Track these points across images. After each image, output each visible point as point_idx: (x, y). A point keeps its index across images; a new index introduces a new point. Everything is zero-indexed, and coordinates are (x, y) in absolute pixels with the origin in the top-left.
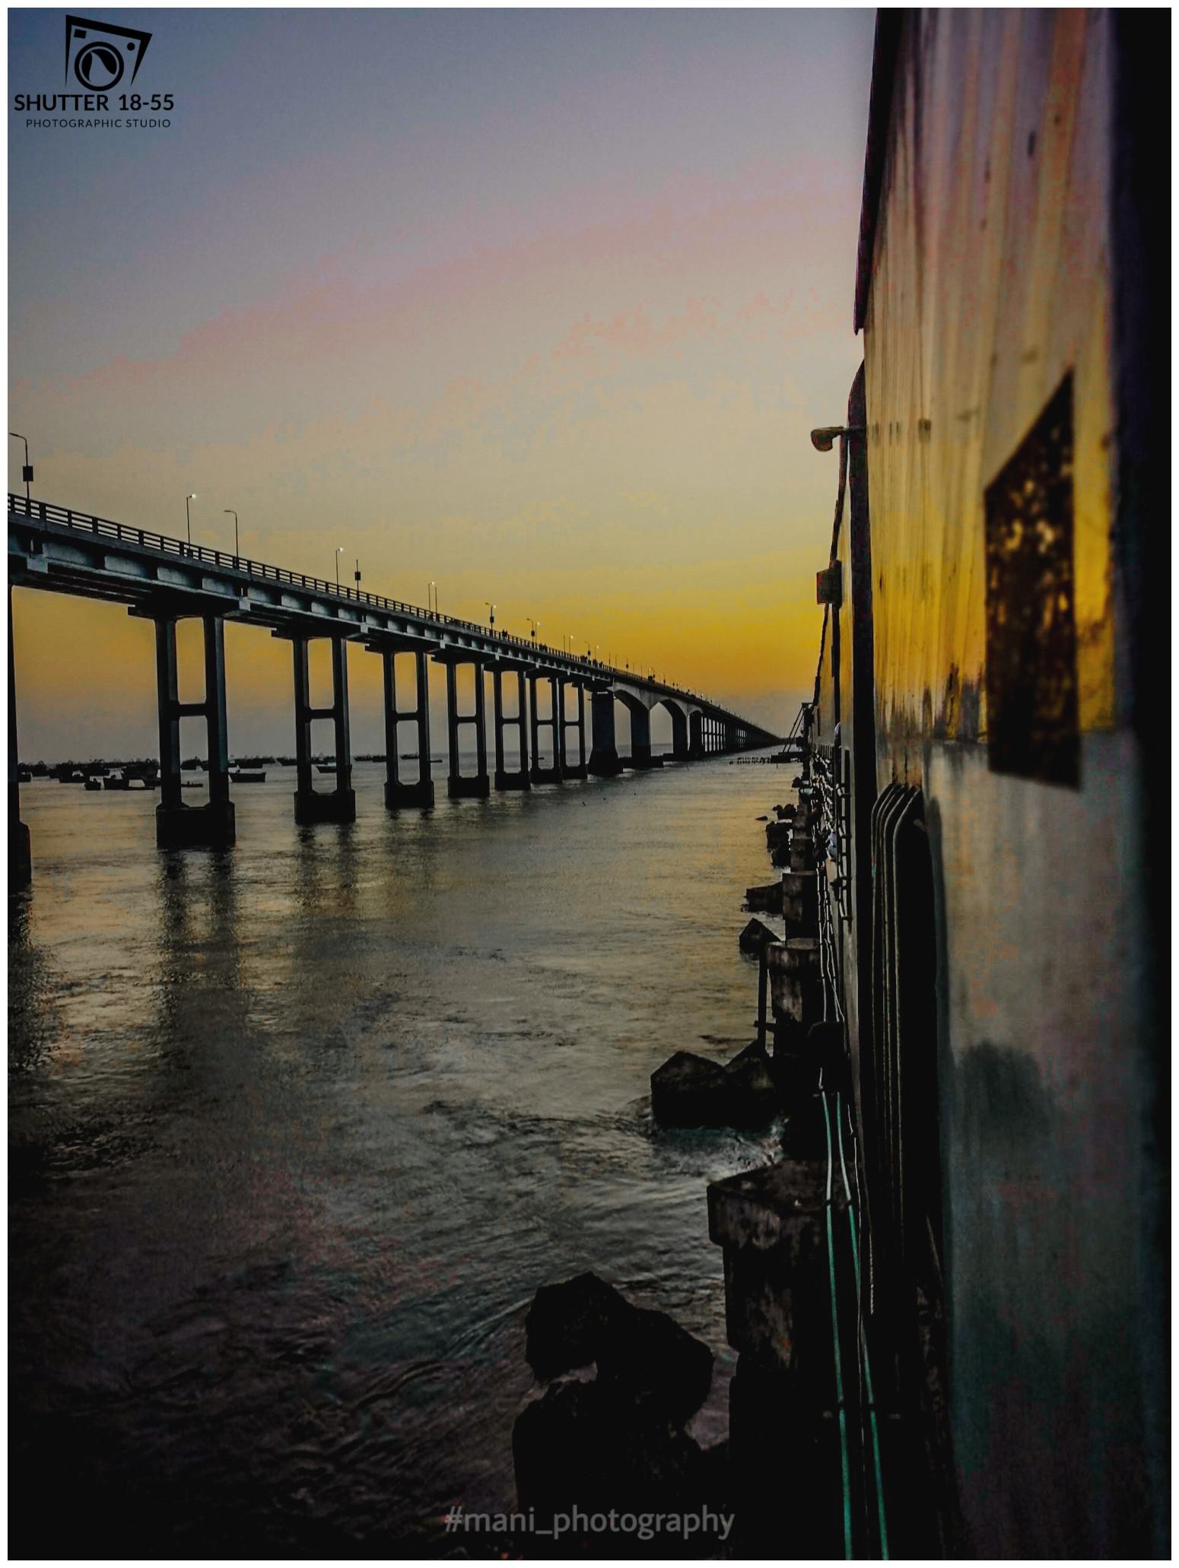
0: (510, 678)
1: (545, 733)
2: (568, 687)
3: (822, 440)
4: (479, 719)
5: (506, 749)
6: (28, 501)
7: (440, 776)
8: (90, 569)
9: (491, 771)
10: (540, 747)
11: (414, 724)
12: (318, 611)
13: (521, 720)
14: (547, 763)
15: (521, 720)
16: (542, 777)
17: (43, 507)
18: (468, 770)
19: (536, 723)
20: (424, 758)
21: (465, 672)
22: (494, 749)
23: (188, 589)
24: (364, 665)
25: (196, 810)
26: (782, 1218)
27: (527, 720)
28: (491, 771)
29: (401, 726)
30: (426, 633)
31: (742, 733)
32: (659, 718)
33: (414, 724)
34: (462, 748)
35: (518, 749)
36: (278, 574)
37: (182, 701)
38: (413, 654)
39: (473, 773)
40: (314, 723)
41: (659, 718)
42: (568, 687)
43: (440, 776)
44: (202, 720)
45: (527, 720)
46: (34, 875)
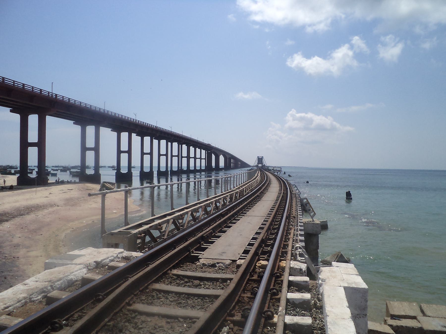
1: (185, 161)
2: (191, 147)
3: (260, 160)
4: (166, 155)
7: (136, 173)
9: (169, 169)
11: (127, 155)
13: (178, 156)
15: (178, 156)
16: (198, 171)
17: (56, 95)
18: (163, 169)
19: (182, 157)
21: (163, 142)
22: (149, 165)
24: (136, 139)
28: (169, 169)
32: (222, 159)
33: (127, 155)
35: (139, 165)
36: (33, 88)
37: (30, 141)
39: (164, 170)
41: (222, 159)
42: (191, 147)
43: (136, 173)
44: (36, 148)
45: (180, 156)
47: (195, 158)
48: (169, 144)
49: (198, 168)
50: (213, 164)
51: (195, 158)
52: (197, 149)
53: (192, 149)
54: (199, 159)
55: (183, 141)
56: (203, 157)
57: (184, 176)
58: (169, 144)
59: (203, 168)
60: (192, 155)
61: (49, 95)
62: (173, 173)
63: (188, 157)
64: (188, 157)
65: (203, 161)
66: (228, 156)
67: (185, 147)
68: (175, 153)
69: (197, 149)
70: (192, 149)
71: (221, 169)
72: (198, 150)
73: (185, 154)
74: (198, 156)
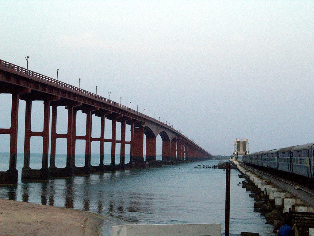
0: (38, 106)
1: (62, 145)
5: (32, 151)
6: (57, 81)
8: (42, 91)
9: (20, 166)
10: (57, 152)
12: (40, 90)
13: (44, 134)
14: (61, 164)
15: (44, 134)
20: (291, 171)
21: (38, 106)
22: (23, 152)
23: (15, 84)
25: (35, 171)
26: (295, 206)
27: (49, 134)
28: (20, 166)
29: (33, 139)
30: (21, 82)
31: (185, 148)
32: (159, 140)
34: (32, 151)
38: (111, 121)
39: (83, 165)
40: (93, 142)
41: (159, 140)
45: (49, 134)
46: (18, 185)
47: (88, 138)
48: (22, 104)
49: (61, 164)
50: (49, 165)
51: (88, 138)
52: (94, 116)
53: (81, 116)
54: (103, 140)
55: (60, 97)
56: (128, 138)
57: (60, 185)
58: (22, 104)
59: (127, 161)
60: (81, 130)
61: (22, 72)
62: (30, 176)
63: (71, 137)
64: (71, 137)
65: (128, 147)
66: (170, 136)
67: (62, 112)
68: (37, 125)
69: (94, 116)
70: (81, 116)
71: (159, 165)
72: (96, 120)
73: (62, 127)
74: (96, 133)
